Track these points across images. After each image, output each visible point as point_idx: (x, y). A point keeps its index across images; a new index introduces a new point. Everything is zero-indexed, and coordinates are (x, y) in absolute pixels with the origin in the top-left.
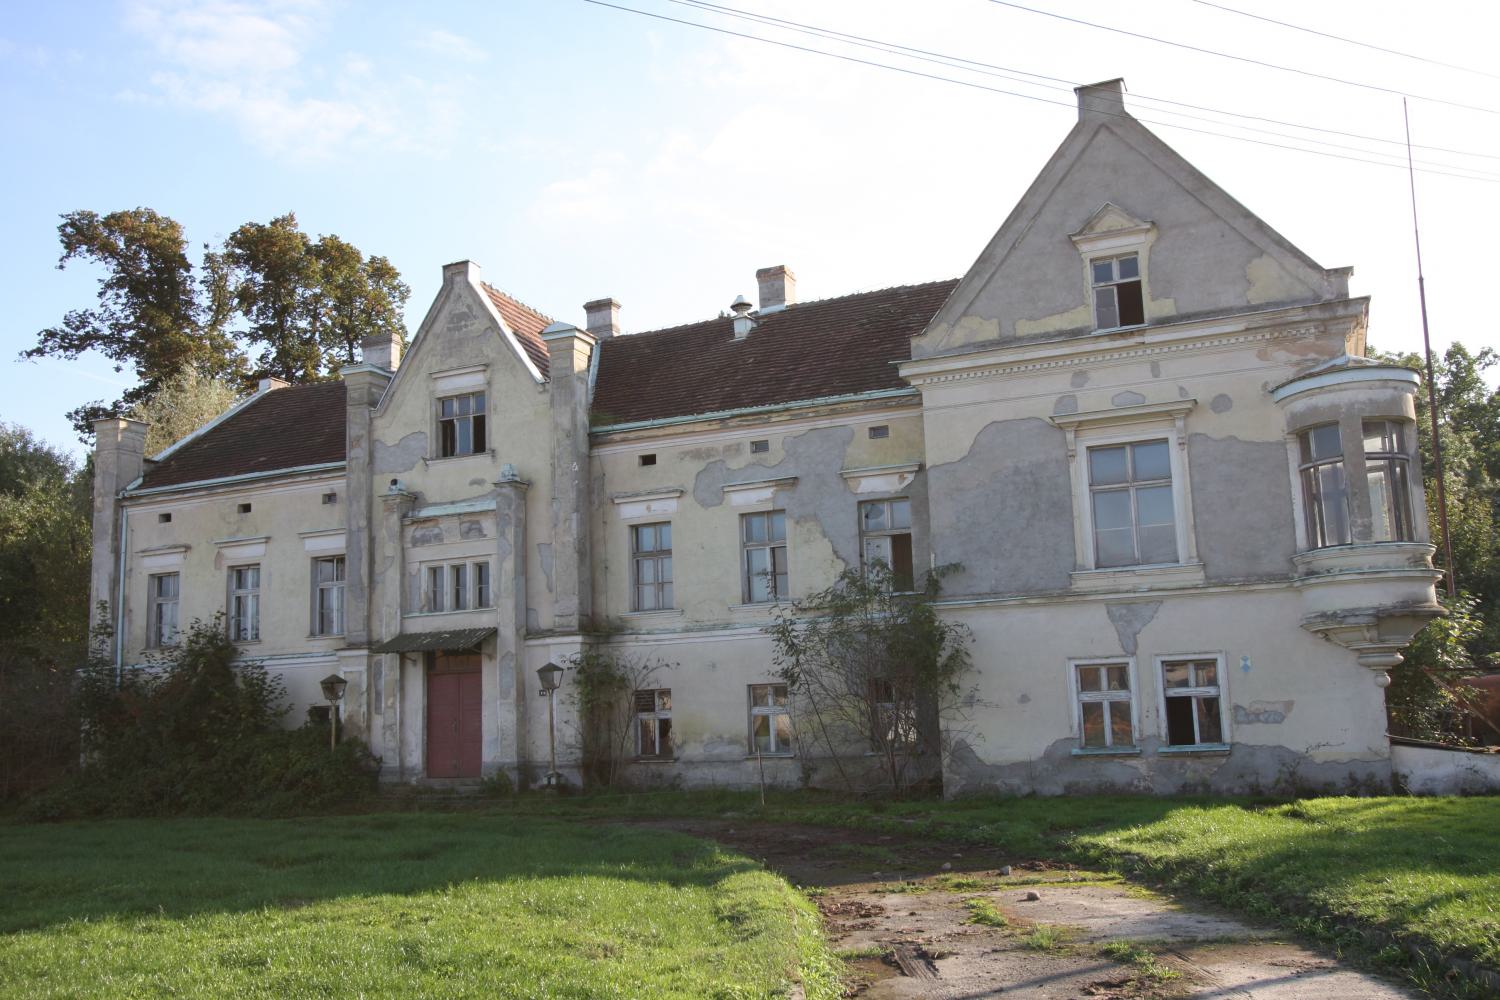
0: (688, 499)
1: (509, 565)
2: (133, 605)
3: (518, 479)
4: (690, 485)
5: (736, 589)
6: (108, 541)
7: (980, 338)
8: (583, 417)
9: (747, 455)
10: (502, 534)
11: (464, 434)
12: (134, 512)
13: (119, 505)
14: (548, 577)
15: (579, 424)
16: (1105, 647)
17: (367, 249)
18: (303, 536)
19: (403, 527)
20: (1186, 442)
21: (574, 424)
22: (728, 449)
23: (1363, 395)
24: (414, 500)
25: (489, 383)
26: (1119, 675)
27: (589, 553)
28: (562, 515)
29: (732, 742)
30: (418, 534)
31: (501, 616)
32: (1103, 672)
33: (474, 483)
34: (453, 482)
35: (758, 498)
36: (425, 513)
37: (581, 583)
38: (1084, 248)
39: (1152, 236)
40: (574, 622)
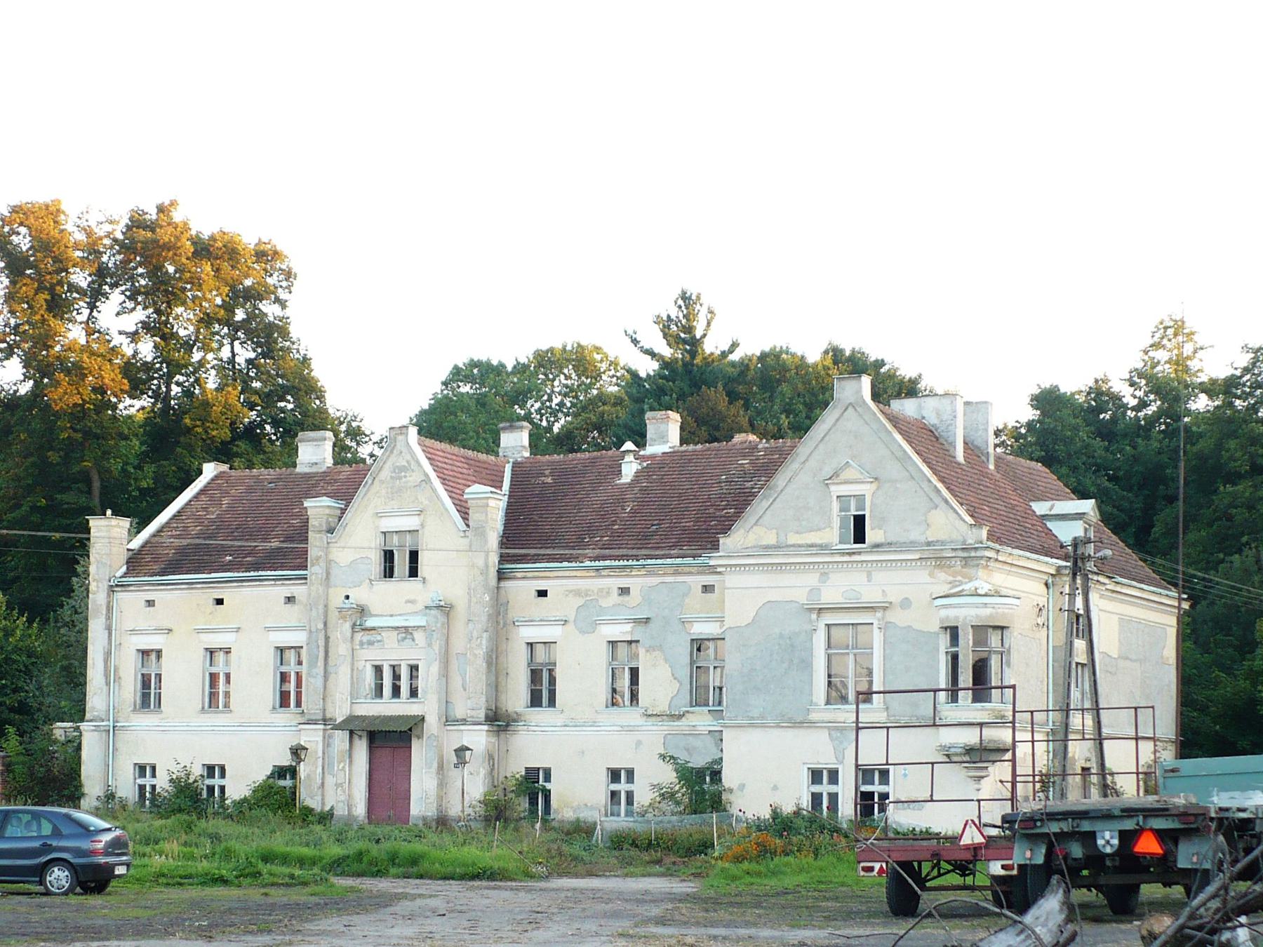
0: (570, 627)
1: (435, 669)
2: (121, 674)
3: (442, 603)
4: (571, 618)
5: (603, 694)
6: (103, 619)
7: (764, 543)
8: (494, 559)
9: (615, 598)
10: (430, 645)
11: (401, 563)
12: (121, 596)
13: (111, 589)
14: (464, 680)
15: (490, 564)
16: (826, 760)
17: (249, 239)
18: (268, 629)
19: (353, 632)
20: (884, 628)
21: (487, 566)
22: (601, 590)
23: (973, 612)
24: (362, 611)
25: (422, 525)
26: (834, 776)
27: (495, 663)
28: (475, 634)
29: (592, 808)
30: (365, 639)
31: (427, 707)
32: (825, 773)
33: (408, 601)
34: (393, 601)
35: (621, 631)
36: (370, 623)
37: (488, 685)
38: (833, 488)
39: (874, 486)
40: (481, 715)
